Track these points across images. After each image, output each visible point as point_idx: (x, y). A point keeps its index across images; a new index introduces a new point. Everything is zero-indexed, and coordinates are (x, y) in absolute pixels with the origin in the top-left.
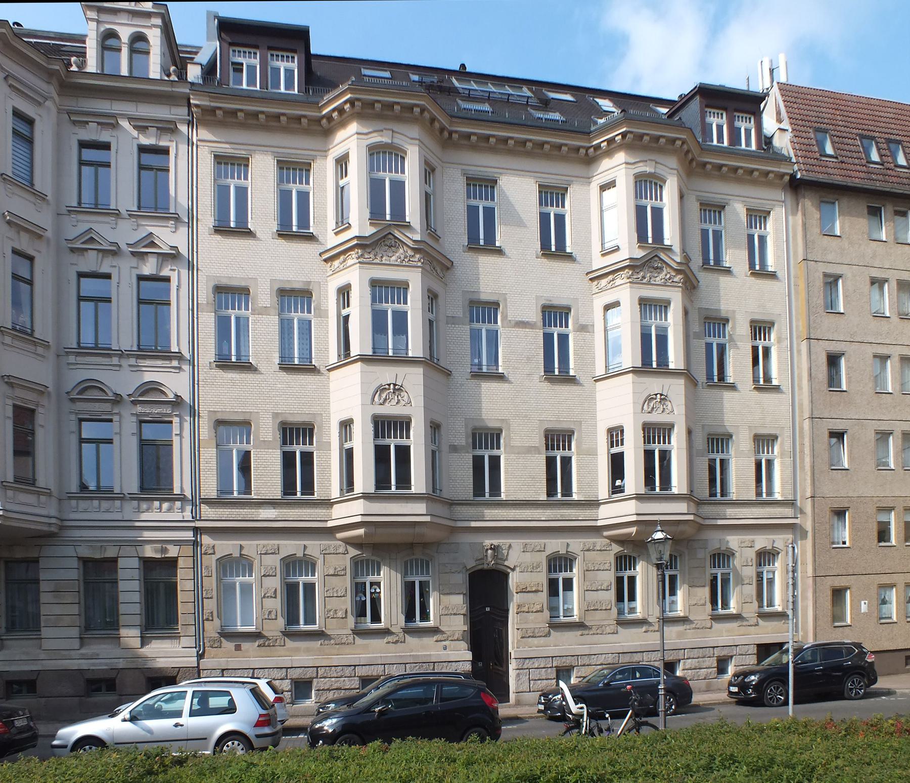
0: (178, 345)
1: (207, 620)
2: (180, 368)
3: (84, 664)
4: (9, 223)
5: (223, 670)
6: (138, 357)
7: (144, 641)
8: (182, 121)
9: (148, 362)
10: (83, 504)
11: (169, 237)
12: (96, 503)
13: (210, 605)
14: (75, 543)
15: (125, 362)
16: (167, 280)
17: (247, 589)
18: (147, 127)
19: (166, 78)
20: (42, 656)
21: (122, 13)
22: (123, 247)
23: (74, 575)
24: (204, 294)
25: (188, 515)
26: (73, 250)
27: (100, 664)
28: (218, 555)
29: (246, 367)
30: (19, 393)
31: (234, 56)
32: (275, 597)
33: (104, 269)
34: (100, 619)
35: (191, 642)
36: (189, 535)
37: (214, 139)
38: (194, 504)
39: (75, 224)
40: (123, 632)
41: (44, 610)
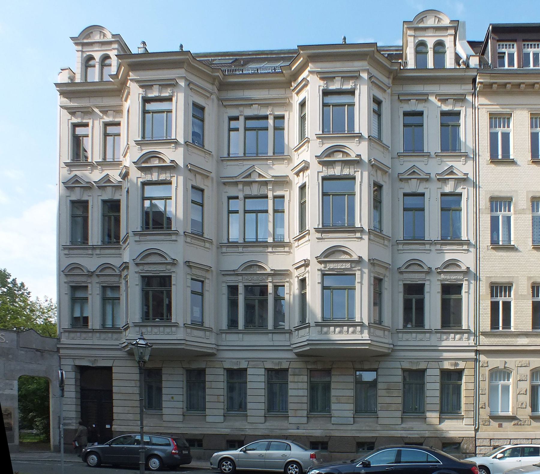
0: (289, 237)
1: (482, 408)
2: (468, 250)
3: (404, 434)
4: (190, 170)
5: (491, 439)
6: (442, 244)
7: (441, 420)
8: (469, 93)
9: (448, 247)
10: (406, 336)
11: (462, 167)
12: (414, 335)
13: (484, 399)
14: (400, 360)
15: (433, 248)
16: (460, 195)
17: (506, 389)
18: (447, 100)
19: (458, 67)
20: (378, 428)
21: (429, 30)
22: (433, 176)
23: (400, 379)
24: (484, 203)
25: (472, 342)
26: (401, 180)
27: (414, 434)
28: (490, 368)
29: (510, 248)
30: (195, 271)
31: (499, 48)
32: (526, 394)
33: (420, 190)
34: (413, 407)
35: (471, 421)
36: (472, 355)
37: (490, 103)
38: (475, 336)
39: (402, 163)
40: (428, 414)
41: (380, 400)
